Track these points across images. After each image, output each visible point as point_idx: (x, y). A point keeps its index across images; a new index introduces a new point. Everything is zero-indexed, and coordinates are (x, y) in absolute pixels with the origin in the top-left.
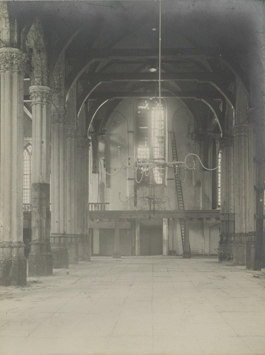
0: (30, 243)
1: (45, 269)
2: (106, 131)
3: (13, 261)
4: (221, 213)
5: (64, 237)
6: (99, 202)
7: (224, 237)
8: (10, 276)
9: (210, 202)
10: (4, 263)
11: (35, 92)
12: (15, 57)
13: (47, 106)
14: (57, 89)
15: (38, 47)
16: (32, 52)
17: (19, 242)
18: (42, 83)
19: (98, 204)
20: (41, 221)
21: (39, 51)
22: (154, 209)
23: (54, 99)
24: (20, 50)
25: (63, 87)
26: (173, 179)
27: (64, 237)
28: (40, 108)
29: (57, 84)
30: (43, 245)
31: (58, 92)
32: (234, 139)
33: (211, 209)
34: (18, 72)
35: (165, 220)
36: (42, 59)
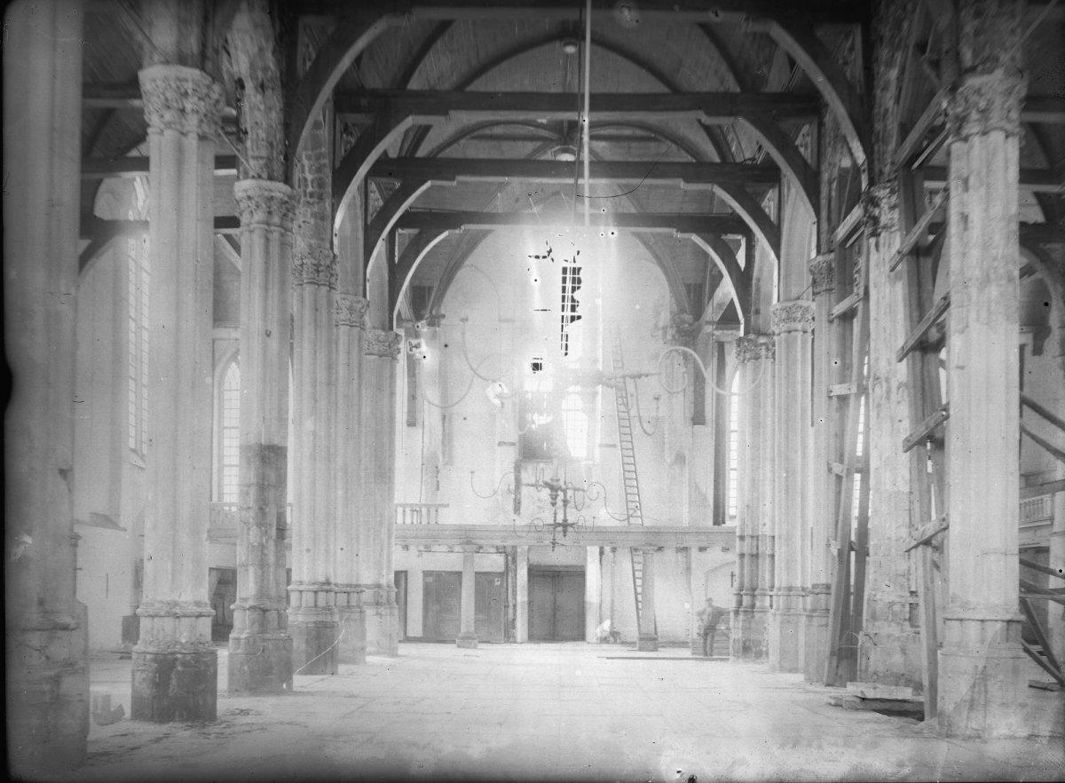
0: (232, 607)
1: (273, 677)
2: (444, 316)
3: (179, 656)
4: (738, 534)
5: (327, 591)
6: (423, 502)
7: (744, 597)
8: (171, 694)
9: (709, 505)
10: (155, 660)
11: (249, 198)
12: (190, 92)
13: (282, 235)
14: (311, 195)
15: (260, 74)
16: (243, 87)
17: (198, 604)
18: (269, 174)
19: (421, 506)
20: (262, 547)
21: (262, 87)
22: (565, 520)
23: (304, 222)
24: (204, 74)
25: (329, 189)
26: (614, 446)
27: (327, 591)
28: (262, 241)
29: (312, 182)
30: (265, 611)
31: (313, 204)
32: (776, 338)
33: (710, 523)
34: (198, 135)
35: (593, 551)
36: (270, 109)
